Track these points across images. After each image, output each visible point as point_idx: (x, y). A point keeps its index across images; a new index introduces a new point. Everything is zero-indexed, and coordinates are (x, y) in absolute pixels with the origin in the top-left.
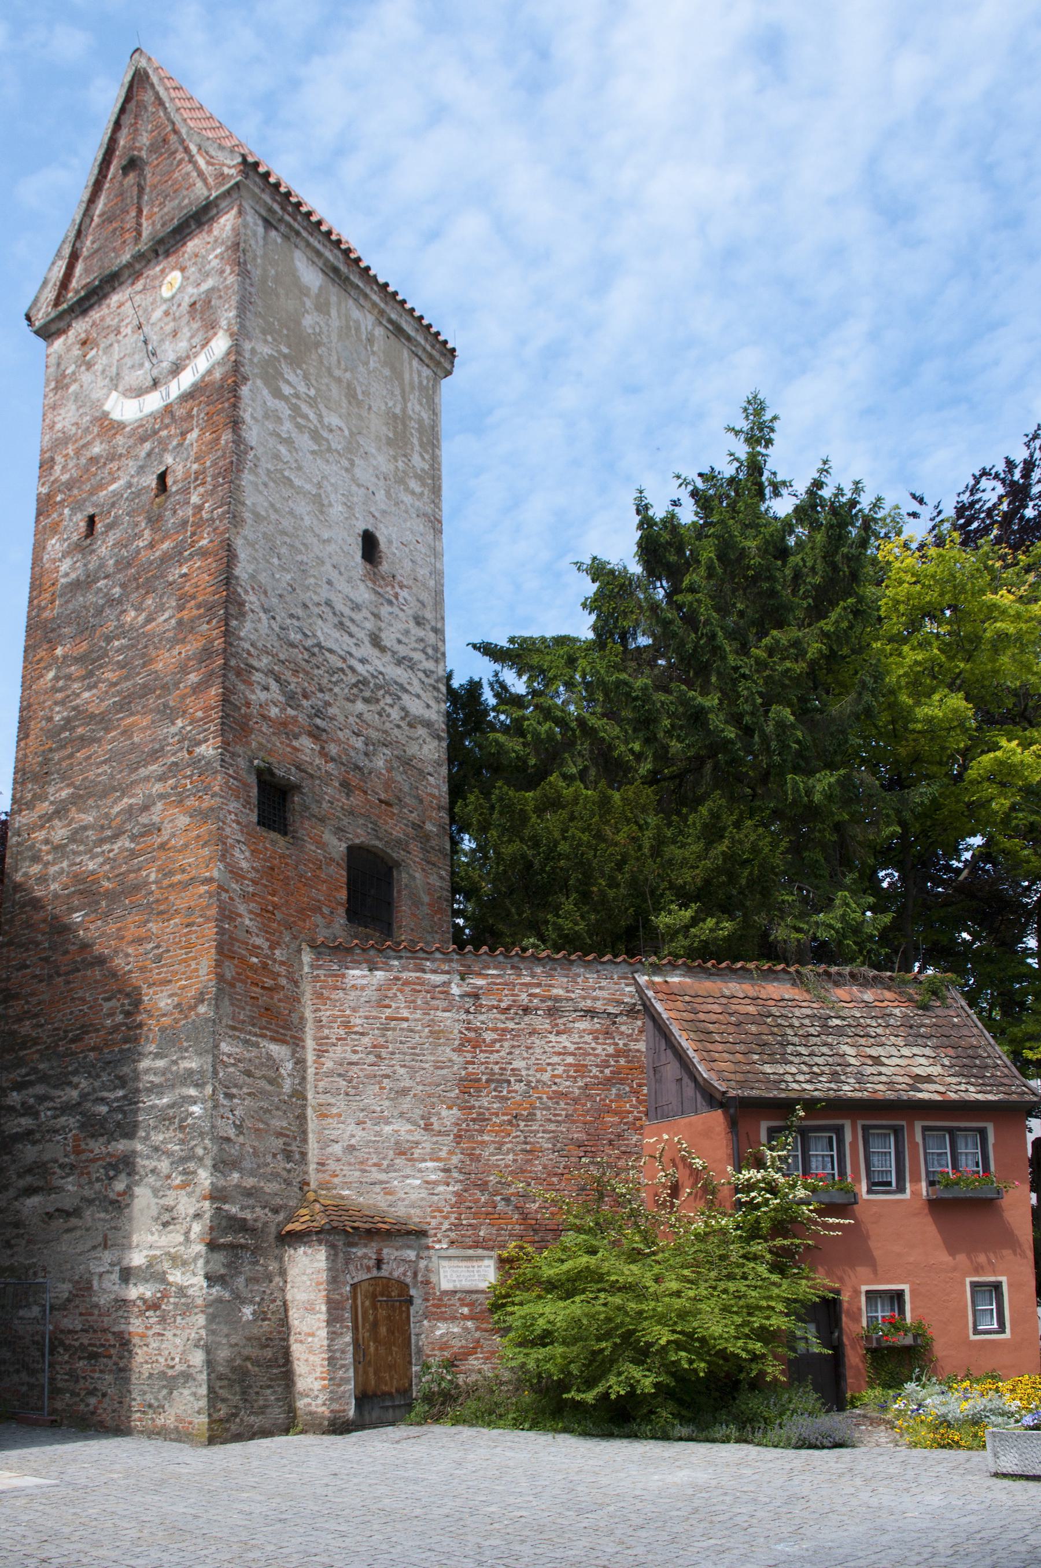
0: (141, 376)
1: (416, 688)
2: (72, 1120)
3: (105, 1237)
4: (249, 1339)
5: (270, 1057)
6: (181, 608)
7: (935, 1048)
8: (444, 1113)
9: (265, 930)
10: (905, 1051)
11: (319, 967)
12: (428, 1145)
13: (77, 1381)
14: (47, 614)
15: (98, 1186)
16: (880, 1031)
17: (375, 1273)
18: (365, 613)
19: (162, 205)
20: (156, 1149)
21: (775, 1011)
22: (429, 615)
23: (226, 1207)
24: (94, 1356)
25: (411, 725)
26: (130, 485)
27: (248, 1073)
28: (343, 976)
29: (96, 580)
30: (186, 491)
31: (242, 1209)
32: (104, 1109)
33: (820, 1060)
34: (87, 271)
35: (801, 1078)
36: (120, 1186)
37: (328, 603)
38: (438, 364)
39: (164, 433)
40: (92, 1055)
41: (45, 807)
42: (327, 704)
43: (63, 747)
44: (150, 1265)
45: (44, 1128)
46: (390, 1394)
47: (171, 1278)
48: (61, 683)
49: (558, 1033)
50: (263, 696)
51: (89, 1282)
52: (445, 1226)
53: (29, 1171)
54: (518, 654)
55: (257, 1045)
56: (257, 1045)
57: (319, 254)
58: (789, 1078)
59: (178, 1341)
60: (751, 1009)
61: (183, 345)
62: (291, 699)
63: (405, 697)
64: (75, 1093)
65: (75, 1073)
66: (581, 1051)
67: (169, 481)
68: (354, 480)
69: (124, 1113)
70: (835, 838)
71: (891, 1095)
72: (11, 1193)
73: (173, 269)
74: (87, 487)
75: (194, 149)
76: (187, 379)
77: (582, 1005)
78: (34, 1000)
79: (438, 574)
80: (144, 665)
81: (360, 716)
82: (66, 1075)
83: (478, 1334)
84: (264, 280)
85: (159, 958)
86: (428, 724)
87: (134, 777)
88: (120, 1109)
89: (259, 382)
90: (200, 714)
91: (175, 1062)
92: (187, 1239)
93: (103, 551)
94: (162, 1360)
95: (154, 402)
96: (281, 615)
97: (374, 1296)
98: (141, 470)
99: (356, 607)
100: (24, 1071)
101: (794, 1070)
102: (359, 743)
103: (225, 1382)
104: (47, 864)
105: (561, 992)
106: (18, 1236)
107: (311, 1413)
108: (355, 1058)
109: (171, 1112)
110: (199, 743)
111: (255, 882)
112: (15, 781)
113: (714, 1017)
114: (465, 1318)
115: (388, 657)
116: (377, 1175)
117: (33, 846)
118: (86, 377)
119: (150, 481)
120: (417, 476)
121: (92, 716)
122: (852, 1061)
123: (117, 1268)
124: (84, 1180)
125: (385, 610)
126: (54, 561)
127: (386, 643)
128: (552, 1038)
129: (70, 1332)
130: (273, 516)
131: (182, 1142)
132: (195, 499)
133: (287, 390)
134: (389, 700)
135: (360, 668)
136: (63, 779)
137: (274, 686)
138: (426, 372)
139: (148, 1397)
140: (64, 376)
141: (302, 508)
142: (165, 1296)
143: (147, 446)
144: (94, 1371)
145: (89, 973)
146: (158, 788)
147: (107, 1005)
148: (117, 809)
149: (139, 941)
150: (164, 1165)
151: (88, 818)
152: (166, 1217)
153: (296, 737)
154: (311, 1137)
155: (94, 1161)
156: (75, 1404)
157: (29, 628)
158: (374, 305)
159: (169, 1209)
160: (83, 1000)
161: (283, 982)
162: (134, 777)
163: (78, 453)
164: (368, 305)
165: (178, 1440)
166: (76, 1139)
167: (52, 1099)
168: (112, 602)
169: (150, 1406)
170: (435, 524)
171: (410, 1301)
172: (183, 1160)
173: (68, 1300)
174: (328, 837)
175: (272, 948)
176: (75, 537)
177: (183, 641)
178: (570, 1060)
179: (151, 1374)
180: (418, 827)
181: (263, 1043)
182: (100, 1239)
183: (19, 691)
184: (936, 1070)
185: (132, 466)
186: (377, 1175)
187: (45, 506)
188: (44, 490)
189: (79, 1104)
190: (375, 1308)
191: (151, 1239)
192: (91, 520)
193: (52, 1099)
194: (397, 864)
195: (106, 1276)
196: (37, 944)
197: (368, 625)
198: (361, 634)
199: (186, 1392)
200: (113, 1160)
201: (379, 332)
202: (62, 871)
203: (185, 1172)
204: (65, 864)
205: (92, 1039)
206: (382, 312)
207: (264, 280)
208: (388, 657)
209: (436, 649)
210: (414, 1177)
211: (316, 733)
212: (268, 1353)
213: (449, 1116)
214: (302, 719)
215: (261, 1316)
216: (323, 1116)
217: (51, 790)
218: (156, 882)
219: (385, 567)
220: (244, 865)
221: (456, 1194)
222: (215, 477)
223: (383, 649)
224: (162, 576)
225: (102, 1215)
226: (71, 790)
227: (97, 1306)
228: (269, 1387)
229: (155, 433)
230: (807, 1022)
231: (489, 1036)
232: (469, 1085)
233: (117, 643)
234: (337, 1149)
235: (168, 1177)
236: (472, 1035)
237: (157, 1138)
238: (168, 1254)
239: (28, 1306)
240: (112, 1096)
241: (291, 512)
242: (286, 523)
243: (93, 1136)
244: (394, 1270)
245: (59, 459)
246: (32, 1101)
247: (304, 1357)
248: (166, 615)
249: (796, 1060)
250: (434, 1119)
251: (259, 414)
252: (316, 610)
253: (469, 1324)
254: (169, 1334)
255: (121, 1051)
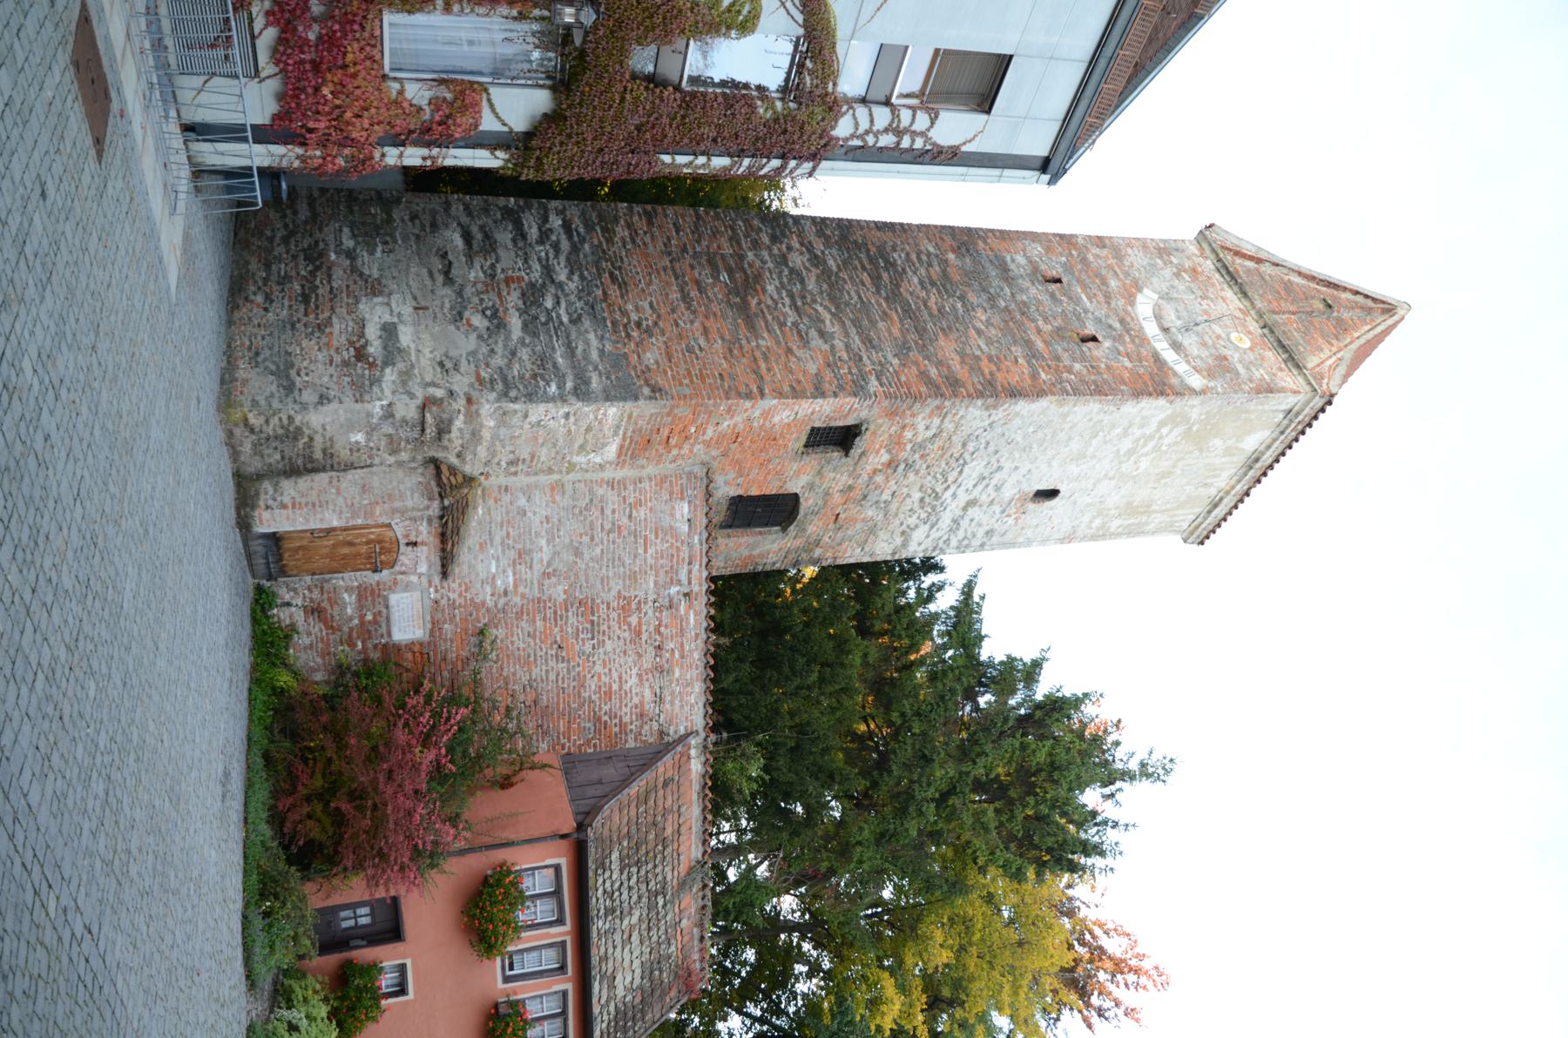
0: (1171, 318)
1: (935, 534)
2: (537, 275)
3: (426, 308)
4: (331, 440)
5: (605, 445)
6: (990, 359)
7: (641, 987)
8: (560, 588)
9: (720, 438)
10: (637, 963)
11: (689, 479)
12: (529, 576)
13: (279, 283)
14: (980, 243)
15: (476, 300)
16: (655, 939)
17: (403, 541)
18: (993, 495)
19: (1298, 330)
20: (513, 354)
21: (669, 849)
22: (995, 539)
23: (461, 417)
24: (306, 299)
25: (903, 533)
26: (1086, 311)
27: (589, 429)
28: (682, 499)
29: (1010, 286)
30: (1083, 358)
31: (460, 430)
32: (549, 304)
33: (625, 896)
34: (1249, 271)
35: (608, 884)
36: (478, 321)
37: (1000, 468)
38: (1192, 533)
39: (1127, 339)
40: (600, 292)
41: (819, 246)
42: (917, 472)
43: (871, 261)
44: (400, 351)
45: (528, 249)
46: (281, 559)
47: (388, 371)
48: (924, 258)
49: (640, 676)
50: (921, 427)
51: (381, 293)
52: (452, 596)
53: (487, 236)
54: (966, 611)
55: (616, 434)
56: (616, 434)
57: (1269, 447)
58: (607, 874)
59: (326, 379)
60: (669, 831)
61: (1194, 350)
62: (921, 446)
63: (927, 527)
64: (562, 277)
65: (582, 277)
66: (624, 695)
67: (1091, 344)
68: (1099, 480)
69: (546, 323)
70: (823, 870)
71: (595, 960)
72: (465, 220)
73: (1252, 340)
74: (1084, 276)
75: (1339, 355)
76: (1169, 356)
77: (666, 692)
78: (648, 239)
79: (1029, 543)
80: (943, 330)
81: (908, 495)
82: (580, 269)
83: (346, 629)
84: (1247, 412)
85: (690, 350)
86: (905, 545)
87: (848, 323)
88: (550, 319)
89: (1169, 412)
90: (903, 378)
91: (596, 368)
92: (428, 385)
93: (1033, 291)
94: (305, 364)
95: (1151, 329)
96: (988, 436)
97: (380, 542)
98: (1098, 321)
99: (998, 488)
100: (582, 230)
101: (615, 877)
102: (886, 496)
103: (285, 421)
104: (769, 249)
105: (677, 674)
106: (423, 226)
107: (257, 494)
108: (608, 512)
109: (549, 366)
110: (878, 379)
111: (761, 427)
112: (840, 220)
113: (660, 803)
114: (362, 617)
115: (959, 512)
116: (499, 536)
117: (784, 236)
118: (1168, 272)
119: (1090, 329)
120: (1104, 524)
121: (898, 286)
122: (626, 922)
123: (395, 320)
124: (480, 287)
125: (997, 509)
126: (1024, 250)
127: (970, 511)
128: (635, 671)
129: (330, 276)
130: (1067, 426)
131: (522, 377)
132: (1077, 366)
133: (1165, 431)
134: (923, 515)
135: (949, 493)
136: (844, 262)
137: (930, 433)
138: (1185, 525)
139: (267, 353)
140: (1169, 254)
141: (1075, 446)
142: (372, 365)
143: (1117, 325)
144: (290, 299)
145: (675, 288)
146: (839, 344)
147: (646, 305)
148: (820, 309)
149: (706, 331)
150: (499, 361)
151: (811, 285)
152: (449, 365)
153: (889, 451)
154: (533, 479)
155: (499, 294)
156: (255, 282)
157: (969, 230)
158: (1233, 487)
159: (456, 367)
160: (650, 283)
161: (675, 452)
162: (848, 323)
163: (1110, 267)
164: (1233, 482)
165: (223, 382)
166: (520, 279)
167: (556, 256)
168: (992, 299)
169: (257, 354)
170: (1068, 539)
171: (375, 571)
172: (505, 380)
173: (361, 275)
174: (804, 479)
175: (704, 442)
176: (1043, 267)
177: (963, 362)
178: (615, 687)
179: (290, 354)
180: (817, 543)
181: (618, 440)
182: (423, 304)
183: (915, 222)
184: (620, 992)
185: (1101, 313)
186: (499, 536)
187: (1067, 240)
188: (1080, 240)
189: (553, 281)
190: (368, 543)
191: (427, 351)
192: (1059, 281)
193: (556, 256)
194: (784, 530)
195: (387, 309)
196: (699, 242)
197: (984, 497)
198: (976, 493)
199: (274, 388)
200: (501, 314)
201: (1213, 491)
202: (765, 263)
203: (492, 381)
204: (770, 265)
205: (614, 291)
206: (1228, 493)
207: (1247, 412)
208: (959, 512)
209: (967, 546)
210: (498, 567)
211: (892, 465)
212: (318, 455)
213: (558, 592)
214: (903, 455)
215: (354, 448)
216: (552, 489)
217: (834, 252)
218: (758, 346)
219: (1031, 506)
220: (776, 419)
221: (483, 603)
222: (1095, 382)
223: (965, 509)
224: (1015, 342)
225: (447, 305)
226: (835, 269)
227: (357, 302)
228: (283, 458)
229: (1128, 332)
230: (660, 878)
231: (634, 620)
232: (587, 607)
233: (959, 305)
234: (522, 502)
235: (487, 365)
236: (634, 606)
237: (524, 354)
238: (413, 366)
239: (354, 236)
240: (562, 311)
241: (1070, 439)
242: (1062, 436)
243: (523, 295)
244: (406, 557)
245: (1105, 251)
246: (554, 238)
247: (315, 485)
248: (984, 347)
249: (625, 876)
250: (554, 580)
251: (1145, 413)
252: (993, 460)
253: (356, 621)
254: (332, 370)
255: (604, 319)
